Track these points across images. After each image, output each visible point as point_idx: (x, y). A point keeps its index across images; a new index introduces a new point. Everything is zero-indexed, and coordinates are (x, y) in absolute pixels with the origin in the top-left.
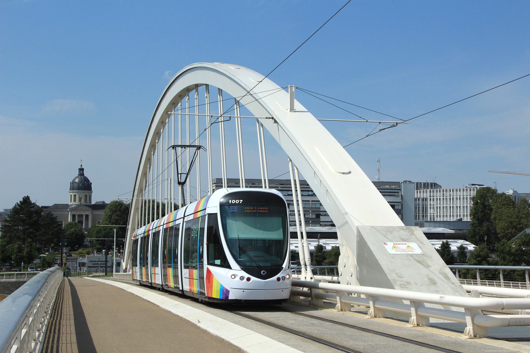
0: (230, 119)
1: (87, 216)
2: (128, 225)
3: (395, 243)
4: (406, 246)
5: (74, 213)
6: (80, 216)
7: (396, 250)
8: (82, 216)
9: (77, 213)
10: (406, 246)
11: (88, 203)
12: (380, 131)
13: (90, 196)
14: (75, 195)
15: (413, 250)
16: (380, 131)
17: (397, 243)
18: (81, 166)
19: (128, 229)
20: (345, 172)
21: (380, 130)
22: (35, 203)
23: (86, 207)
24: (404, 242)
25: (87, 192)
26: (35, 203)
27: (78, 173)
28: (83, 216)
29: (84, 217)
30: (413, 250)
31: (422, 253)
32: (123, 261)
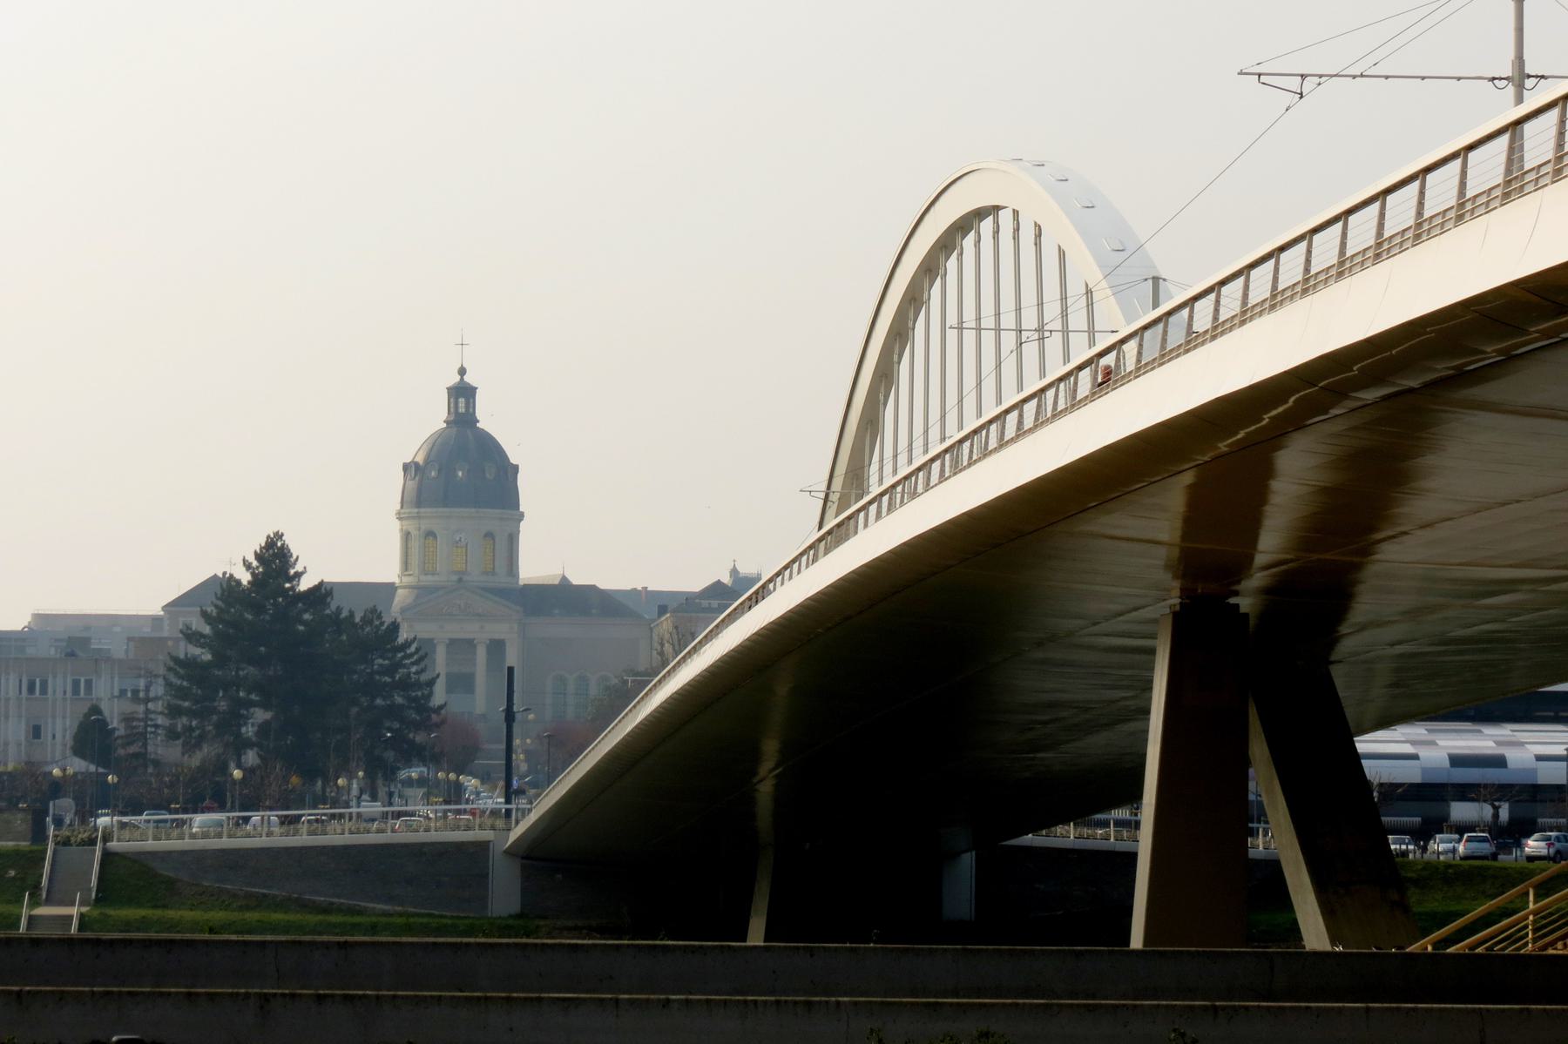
1: (496, 647)
8: (471, 644)
18: (462, 371)
27: (443, 414)
28: (475, 646)
29: (481, 654)
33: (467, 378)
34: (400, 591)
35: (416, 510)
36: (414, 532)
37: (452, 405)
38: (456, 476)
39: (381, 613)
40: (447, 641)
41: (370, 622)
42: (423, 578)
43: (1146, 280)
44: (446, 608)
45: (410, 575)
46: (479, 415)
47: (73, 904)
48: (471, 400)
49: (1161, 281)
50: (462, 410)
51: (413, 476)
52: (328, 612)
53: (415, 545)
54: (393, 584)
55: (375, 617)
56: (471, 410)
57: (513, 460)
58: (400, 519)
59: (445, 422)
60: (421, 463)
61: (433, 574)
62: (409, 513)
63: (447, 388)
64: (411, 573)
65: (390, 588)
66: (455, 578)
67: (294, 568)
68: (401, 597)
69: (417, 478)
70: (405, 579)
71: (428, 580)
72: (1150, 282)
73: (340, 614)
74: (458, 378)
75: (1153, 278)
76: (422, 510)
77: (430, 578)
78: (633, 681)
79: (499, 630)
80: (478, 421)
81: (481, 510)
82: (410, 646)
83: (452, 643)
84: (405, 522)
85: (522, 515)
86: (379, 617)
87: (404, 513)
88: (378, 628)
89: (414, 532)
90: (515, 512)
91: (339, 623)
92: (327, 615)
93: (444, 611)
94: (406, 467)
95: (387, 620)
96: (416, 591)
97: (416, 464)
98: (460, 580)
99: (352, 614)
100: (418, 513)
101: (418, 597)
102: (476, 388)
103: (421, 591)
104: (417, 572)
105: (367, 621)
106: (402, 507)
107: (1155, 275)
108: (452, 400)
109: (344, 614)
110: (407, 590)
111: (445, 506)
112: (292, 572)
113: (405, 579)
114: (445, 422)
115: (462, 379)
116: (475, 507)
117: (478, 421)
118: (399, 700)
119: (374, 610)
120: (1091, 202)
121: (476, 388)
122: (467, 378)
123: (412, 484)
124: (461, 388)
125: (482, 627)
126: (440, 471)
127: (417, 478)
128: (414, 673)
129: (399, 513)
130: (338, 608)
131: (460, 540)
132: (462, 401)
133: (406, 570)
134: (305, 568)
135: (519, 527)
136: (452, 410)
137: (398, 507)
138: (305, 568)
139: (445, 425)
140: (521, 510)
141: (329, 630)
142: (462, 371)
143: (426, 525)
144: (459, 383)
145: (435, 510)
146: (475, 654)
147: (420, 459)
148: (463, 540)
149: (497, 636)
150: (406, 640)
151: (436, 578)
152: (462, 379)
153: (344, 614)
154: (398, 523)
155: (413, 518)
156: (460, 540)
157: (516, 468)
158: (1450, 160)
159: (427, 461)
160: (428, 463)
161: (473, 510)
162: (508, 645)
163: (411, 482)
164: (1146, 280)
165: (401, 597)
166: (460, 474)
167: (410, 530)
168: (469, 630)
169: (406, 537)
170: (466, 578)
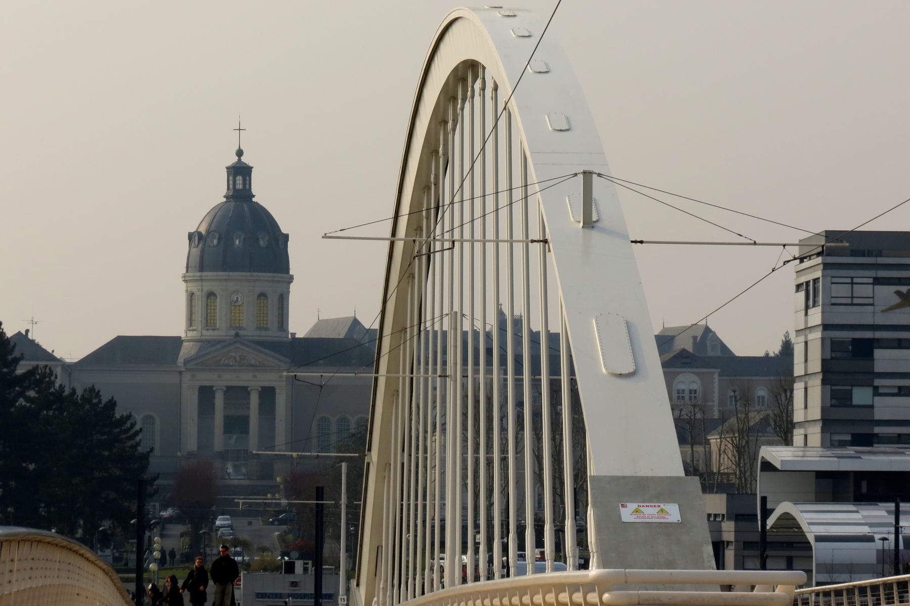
0: (454, 246)
1: (268, 394)
2: (370, 450)
3: (639, 504)
4: (658, 509)
5: (207, 378)
6: (237, 394)
7: (636, 516)
8: (244, 391)
9: (221, 380)
10: (658, 509)
11: (272, 334)
12: (784, 264)
13: (283, 300)
14: (211, 295)
15: (667, 517)
16: (784, 264)
17: (645, 505)
18: (240, 153)
19: (368, 464)
20: (622, 373)
21: (784, 262)
22: (27, 331)
23: (259, 348)
24: (652, 503)
25: (263, 280)
26: (27, 331)
27: (223, 190)
28: (249, 393)
29: (254, 399)
30: (667, 517)
31: (679, 521)
32: (358, 585)
33: (244, 159)
34: (185, 344)
35: (199, 274)
36: (197, 293)
37: (231, 182)
38: (233, 244)
39: (99, 391)
40: (225, 389)
41: (89, 401)
42: (205, 333)
43: (576, 175)
44: (224, 359)
45: (194, 330)
46: (254, 190)
47: (373, 373)
48: (248, 178)
49: (594, 176)
50: (239, 186)
51: (197, 244)
52: (52, 390)
53: (199, 305)
54: (180, 337)
55: (94, 395)
56: (247, 186)
57: (284, 230)
58: (185, 281)
59: (224, 197)
60: (203, 233)
61: (213, 330)
62: (194, 276)
63: (227, 168)
64: (195, 328)
65: (176, 342)
66: (233, 332)
67: (11, 354)
68: (187, 350)
69: (200, 246)
70: (190, 334)
71: (209, 334)
72: (581, 177)
73: (64, 392)
74: (236, 159)
75: (584, 173)
76: (204, 274)
77: (210, 333)
78: (243, 504)
79: (267, 379)
80: (254, 196)
81: (255, 274)
82: (125, 423)
83: (229, 391)
84: (189, 284)
85: (291, 278)
86: (98, 395)
87: (189, 276)
88: (96, 405)
89: (197, 293)
90: (284, 275)
91: (60, 400)
92: (52, 394)
93: (222, 362)
94: (191, 236)
95: (105, 399)
96: (199, 344)
97: (200, 234)
98: (237, 335)
99: (74, 392)
100: (200, 276)
101: (200, 350)
102: (252, 167)
103: (205, 344)
104: (199, 329)
105: (86, 399)
106: (187, 271)
107: (587, 168)
108: (231, 178)
109: (67, 392)
110: (191, 343)
111: (224, 270)
112: (10, 358)
113: (190, 334)
114: (224, 197)
115: (239, 160)
116: (250, 271)
117: (254, 196)
118: (117, 472)
119: (92, 389)
120: (547, 65)
121: (252, 167)
122: (244, 159)
123: (196, 251)
124: (238, 168)
125: (255, 376)
126: (219, 239)
127: (200, 246)
128: (130, 447)
129: (184, 276)
130: (61, 386)
131: (237, 300)
132: (239, 179)
133: (191, 326)
134: (22, 354)
135: (289, 288)
136: (231, 187)
137: (184, 271)
138: (22, 354)
139: (225, 200)
140: (291, 273)
141: (54, 407)
142: (240, 153)
143: (208, 287)
144: (237, 163)
145: (215, 273)
146: (249, 399)
147: (203, 230)
148: (239, 300)
149: (267, 384)
150: (122, 417)
151: (216, 333)
152: (239, 160)
153: (67, 392)
154: (184, 284)
155: (197, 280)
156: (237, 300)
157: (286, 237)
158: (282, 305)
159: (209, 232)
160: (210, 233)
161: (249, 274)
162: (277, 391)
163: (196, 249)
164: (576, 175)
165: (187, 350)
166: (237, 242)
167: (194, 291)
168: (243, 379)
169: (191, 296)
170: (241, 333)
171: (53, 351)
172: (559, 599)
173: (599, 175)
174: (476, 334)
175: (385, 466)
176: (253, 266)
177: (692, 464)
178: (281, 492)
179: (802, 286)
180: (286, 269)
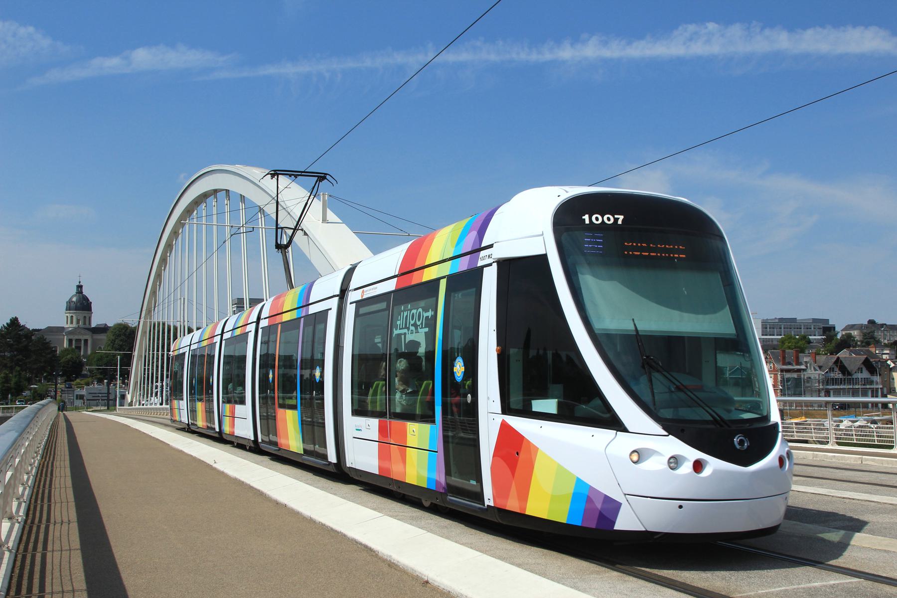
1: (86, 341)
2: (134, 351)
6: (78, 341)
8: (80, 340)
11: (87, 326)
14: (72, 317)
18: (80, 282)
25: (85, 313)
29: (83, 342)
32: (128, 393)
142: (80, 282)
171: (82, 305)
172: (441, 280)
173: (305, 234)
174: (159, 324)
175: (140, 356)
176: (83, 310)
177: (17, 482)
178: (49, 389)
179: (66, 415)
180: (91, 311)
